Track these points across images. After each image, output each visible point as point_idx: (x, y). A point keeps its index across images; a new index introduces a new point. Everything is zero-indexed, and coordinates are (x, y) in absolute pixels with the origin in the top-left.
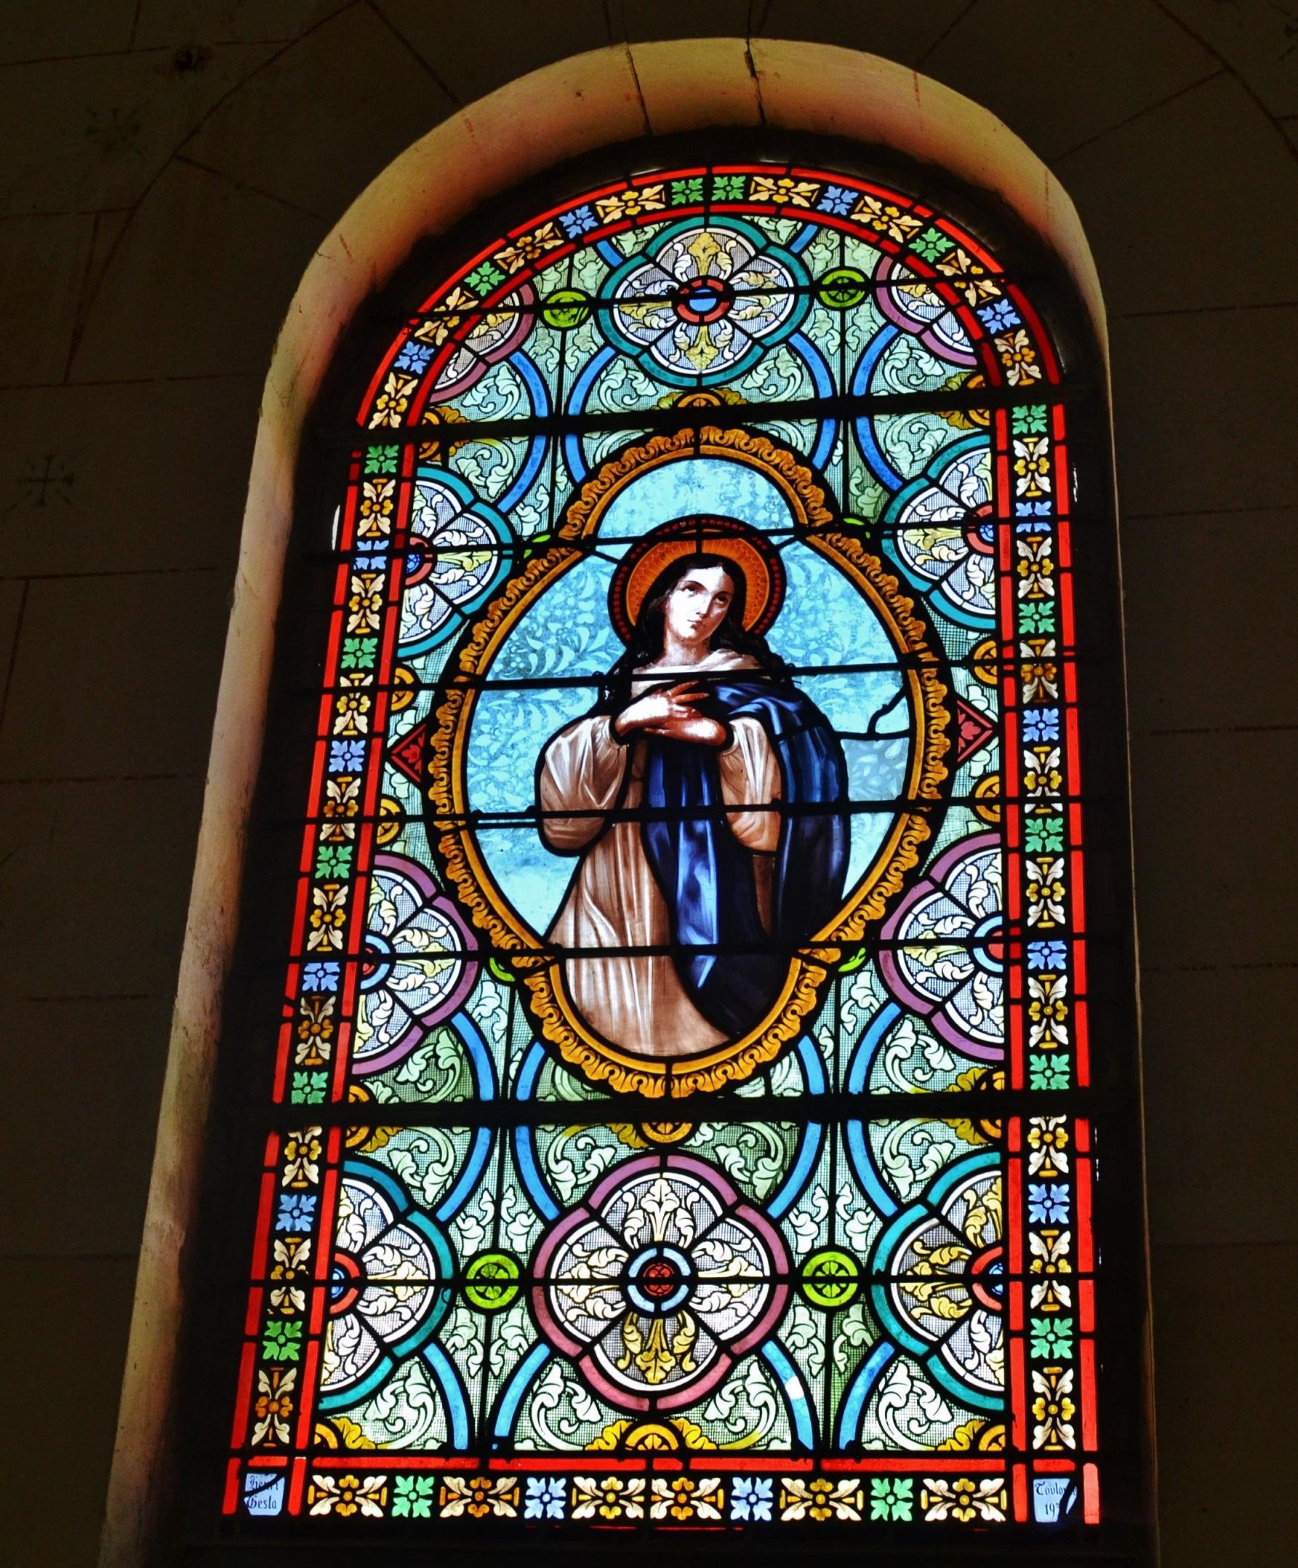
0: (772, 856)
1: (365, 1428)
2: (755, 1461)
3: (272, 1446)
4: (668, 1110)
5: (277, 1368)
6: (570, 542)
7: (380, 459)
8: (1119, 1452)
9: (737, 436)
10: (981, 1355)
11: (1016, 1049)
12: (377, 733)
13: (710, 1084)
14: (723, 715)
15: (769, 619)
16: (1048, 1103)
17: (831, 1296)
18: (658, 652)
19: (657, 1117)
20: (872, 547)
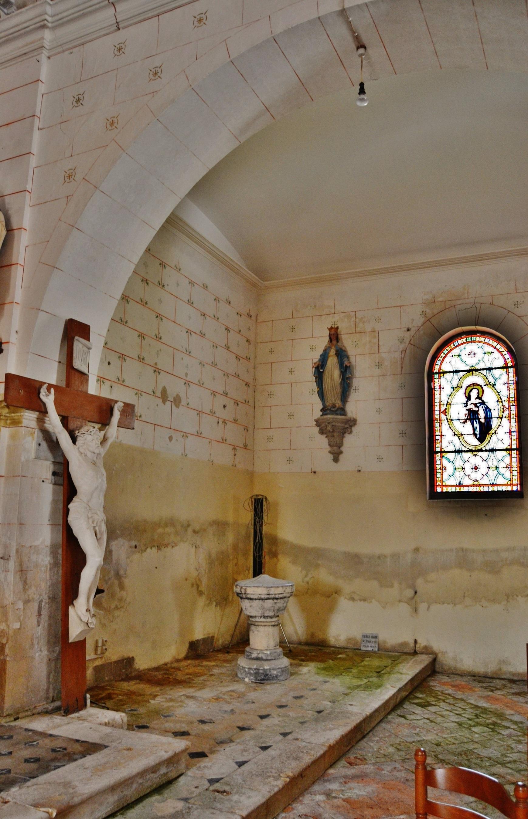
0: (484, 423)
1: (448, 483)
2: (486, 485)
3: (439, 485)
4: (475, 451)
5: (438, 477)
6: (459, 387)
7: (436, 376)
8: (521, 484)
9: (477, 373)
10: (508, 474)
11: (511, 445)
12: (440, 410)
13: (479, 448)
14: (478, 407)
15: (482, 396)
16: (514, 449)
17: (493, 469)
18: (470, 400)
19: (474, 451)
20: (493, 387)
